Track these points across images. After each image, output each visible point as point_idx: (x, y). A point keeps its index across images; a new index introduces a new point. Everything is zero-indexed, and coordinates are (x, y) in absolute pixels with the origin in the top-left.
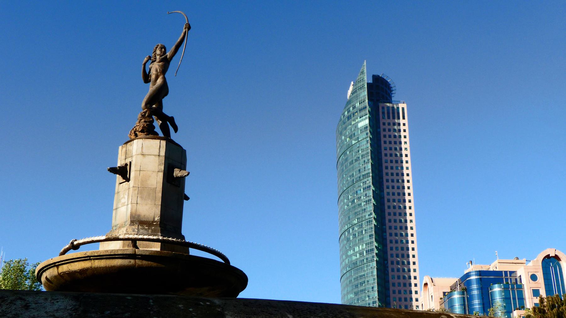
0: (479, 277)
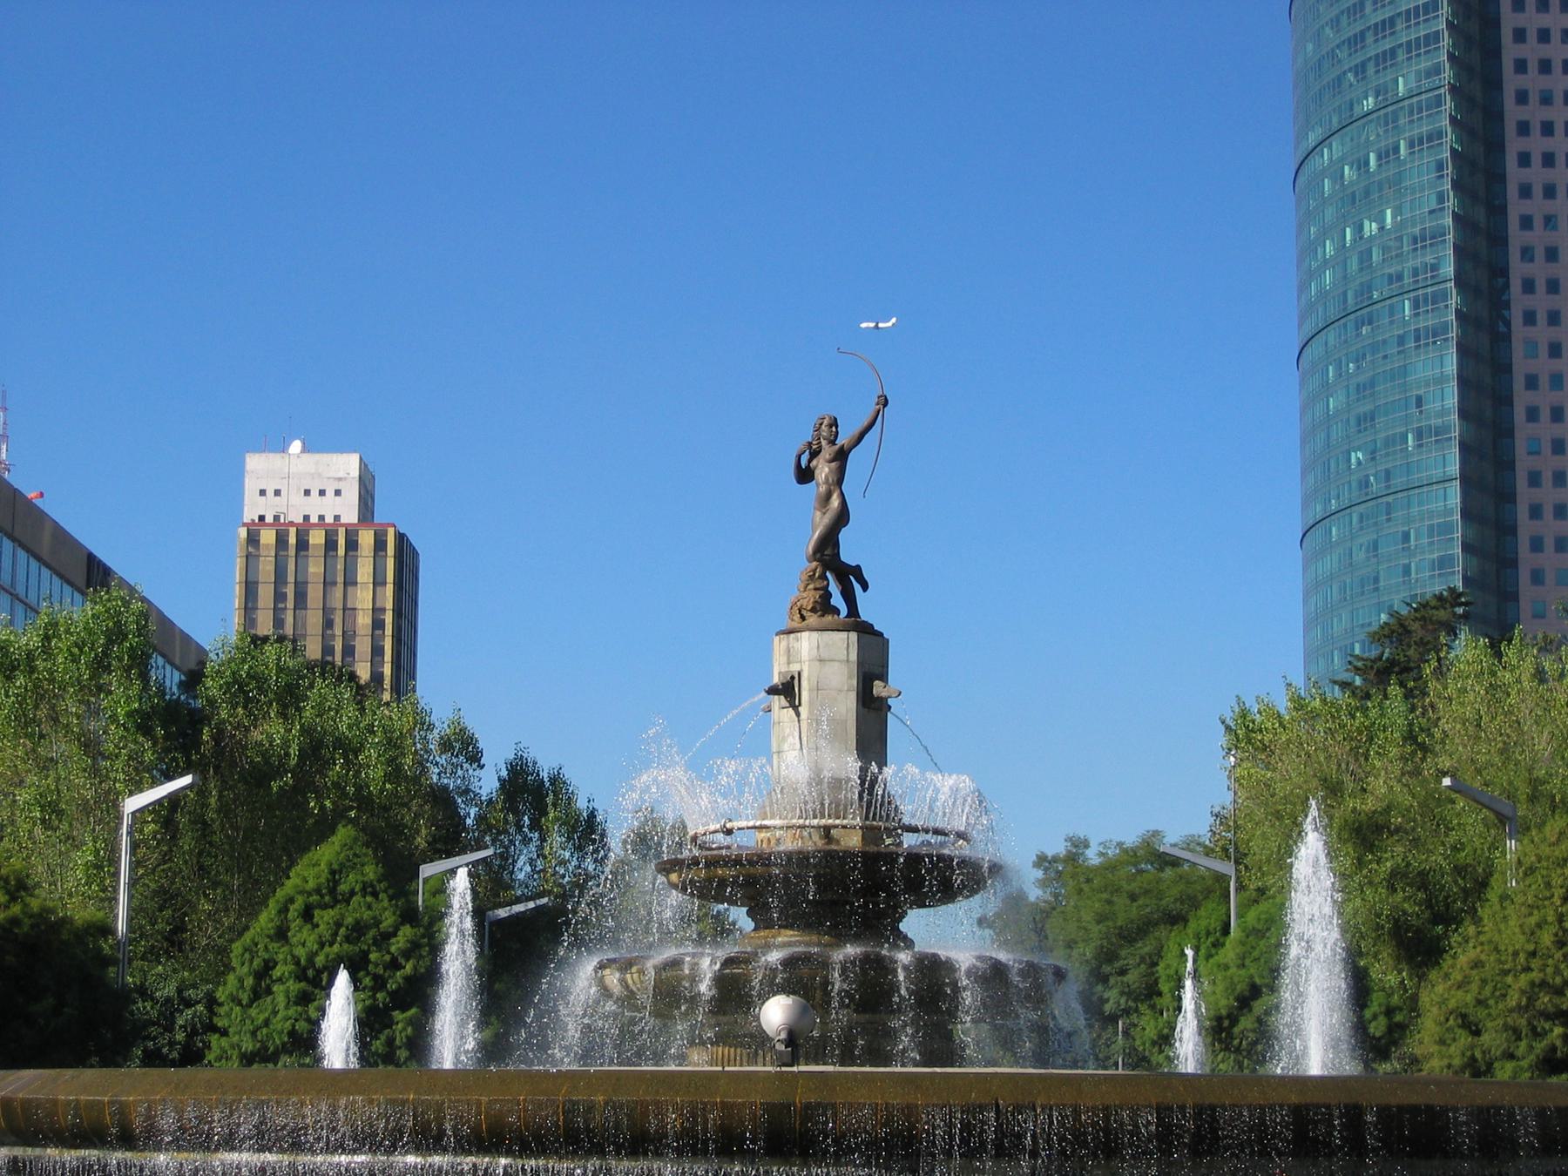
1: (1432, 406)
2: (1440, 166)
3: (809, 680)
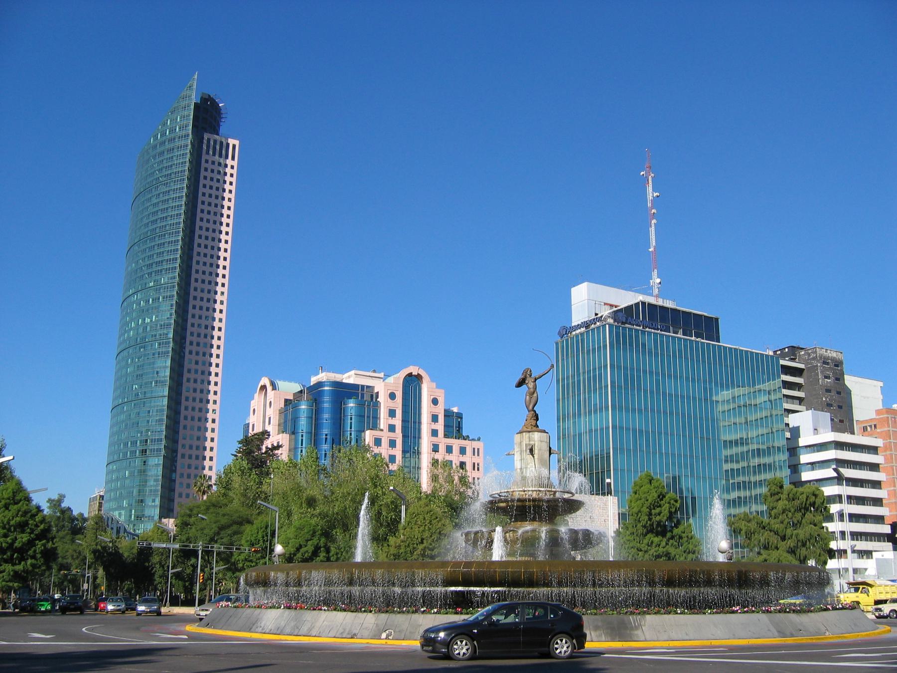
0: (331, 388)
1: (162, 374)
2: (172, 305)
3: (538, 446)
